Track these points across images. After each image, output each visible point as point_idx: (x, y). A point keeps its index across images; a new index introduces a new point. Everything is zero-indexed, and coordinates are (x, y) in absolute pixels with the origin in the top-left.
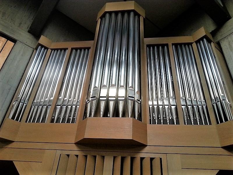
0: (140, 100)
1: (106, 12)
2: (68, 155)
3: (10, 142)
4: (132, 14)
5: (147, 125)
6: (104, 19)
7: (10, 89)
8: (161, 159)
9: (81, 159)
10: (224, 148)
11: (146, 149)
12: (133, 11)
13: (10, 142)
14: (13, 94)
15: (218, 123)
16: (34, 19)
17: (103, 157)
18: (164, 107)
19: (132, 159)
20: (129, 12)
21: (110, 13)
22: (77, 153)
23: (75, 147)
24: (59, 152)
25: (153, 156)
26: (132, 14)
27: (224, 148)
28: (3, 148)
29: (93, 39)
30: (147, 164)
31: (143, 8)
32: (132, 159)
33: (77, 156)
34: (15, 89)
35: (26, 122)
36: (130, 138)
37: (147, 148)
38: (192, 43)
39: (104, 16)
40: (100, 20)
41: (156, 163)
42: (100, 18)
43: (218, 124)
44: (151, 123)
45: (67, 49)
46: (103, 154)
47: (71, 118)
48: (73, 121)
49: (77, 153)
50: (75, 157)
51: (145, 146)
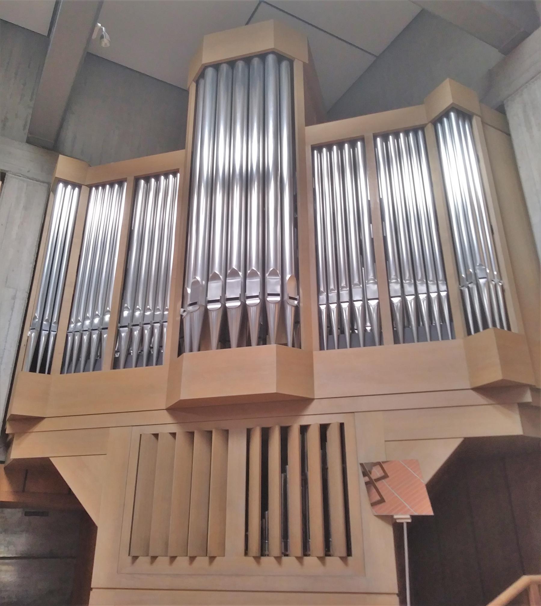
0: (297, 297)
1: (205, 68)
2: (156, 436)
3: (38, 420)
4: (271, 59)
5: (315, 353)
6: (202, 82)
7: (14, 298)
8: (342, 425)
9: (181, 438)
10: (478, 390)
11: (313, 408)
12: (273, 52)
13: (38, 420)
14: (23, 308)
15: (469, 333)
16: (24, 556)
17: (226, 433)
18: (367, 302)
19: (285, 432)
20: (263, 56)
21: (216, 66)
22: (174, 428)
23: (167, 418)
24: (136, 431)
25: (324, 420)
26: (271, 59)
27: (478, 390)
28: (28, 434)
29: (183, 146)
30: (313, 437)
31: (13, 508)
32: (285, 432)
33: (174, 435)
34: (26, 295)
35: (62, 372)
36: (274, 391)
37: (314, 404)
38: (425, 125)
39: (202, 75)
40: (194, 85)
41: (333, 435)
42: (193, 80)
43: (470, 337)
44: (321, 348)
45: (125, 180)
46: (225, 425)
47: (155, 352)
48: (159, 361)
49: (174, 428)
50: (170, 437)
51: (310, 400)
